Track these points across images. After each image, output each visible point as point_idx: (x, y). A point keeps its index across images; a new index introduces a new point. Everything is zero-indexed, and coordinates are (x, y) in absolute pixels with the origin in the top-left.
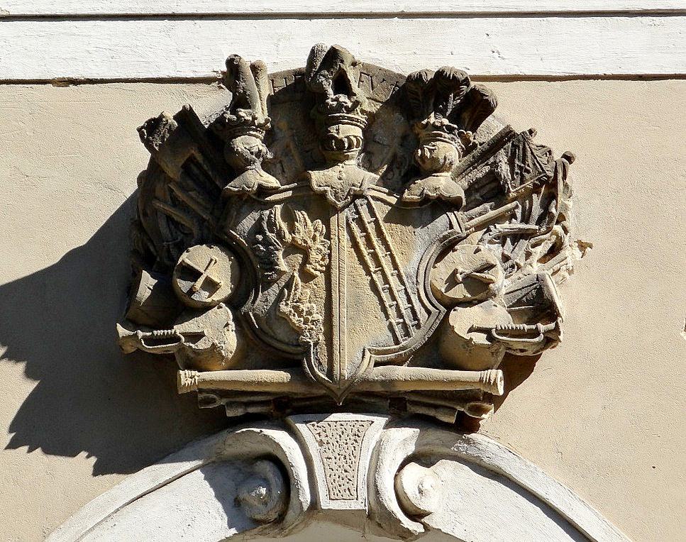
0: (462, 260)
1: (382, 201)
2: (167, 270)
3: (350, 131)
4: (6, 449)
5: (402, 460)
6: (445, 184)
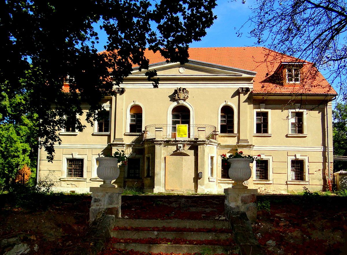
0: (185, 95)
1: (182, 93)
2: (175, 95)
3: (181, 90)
4: (243, 102)
5: (321, 120)
6: (185, 92)
